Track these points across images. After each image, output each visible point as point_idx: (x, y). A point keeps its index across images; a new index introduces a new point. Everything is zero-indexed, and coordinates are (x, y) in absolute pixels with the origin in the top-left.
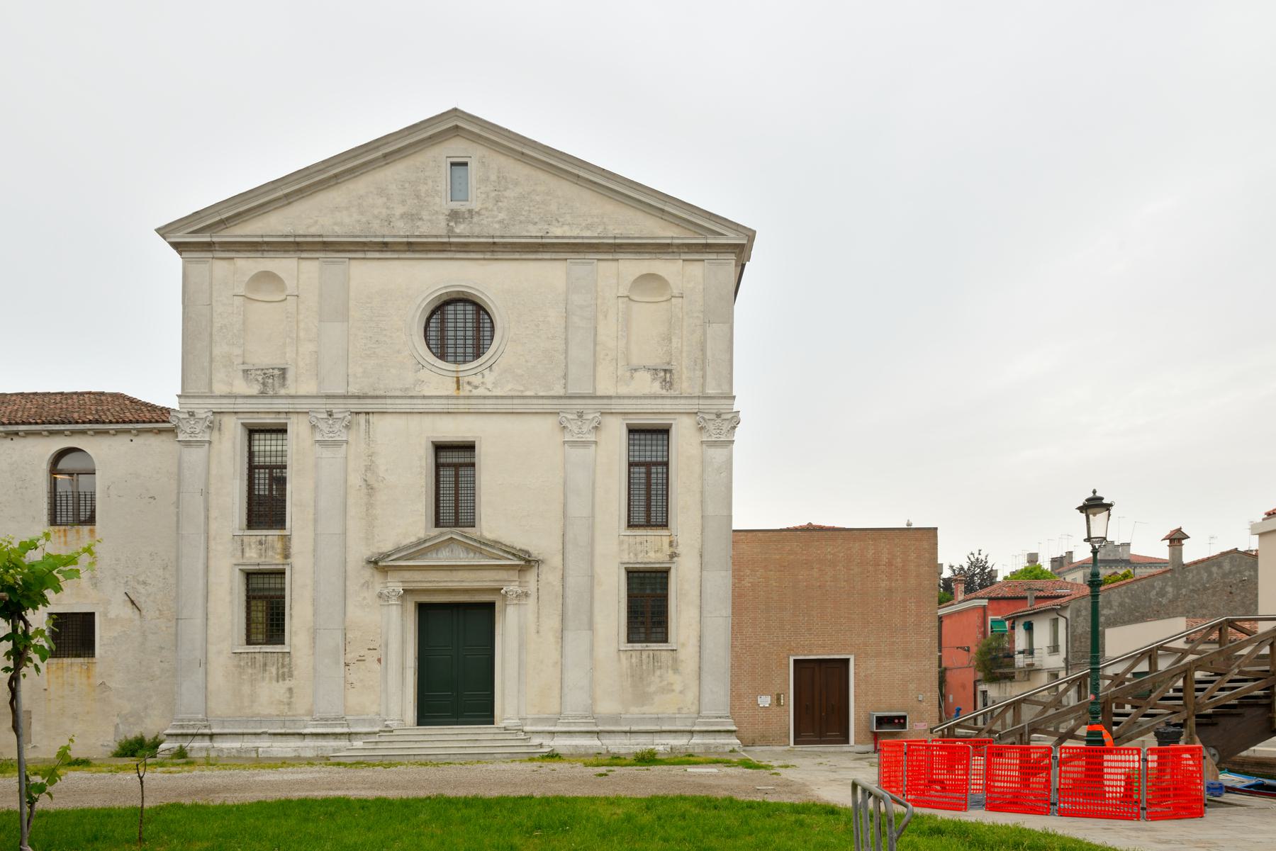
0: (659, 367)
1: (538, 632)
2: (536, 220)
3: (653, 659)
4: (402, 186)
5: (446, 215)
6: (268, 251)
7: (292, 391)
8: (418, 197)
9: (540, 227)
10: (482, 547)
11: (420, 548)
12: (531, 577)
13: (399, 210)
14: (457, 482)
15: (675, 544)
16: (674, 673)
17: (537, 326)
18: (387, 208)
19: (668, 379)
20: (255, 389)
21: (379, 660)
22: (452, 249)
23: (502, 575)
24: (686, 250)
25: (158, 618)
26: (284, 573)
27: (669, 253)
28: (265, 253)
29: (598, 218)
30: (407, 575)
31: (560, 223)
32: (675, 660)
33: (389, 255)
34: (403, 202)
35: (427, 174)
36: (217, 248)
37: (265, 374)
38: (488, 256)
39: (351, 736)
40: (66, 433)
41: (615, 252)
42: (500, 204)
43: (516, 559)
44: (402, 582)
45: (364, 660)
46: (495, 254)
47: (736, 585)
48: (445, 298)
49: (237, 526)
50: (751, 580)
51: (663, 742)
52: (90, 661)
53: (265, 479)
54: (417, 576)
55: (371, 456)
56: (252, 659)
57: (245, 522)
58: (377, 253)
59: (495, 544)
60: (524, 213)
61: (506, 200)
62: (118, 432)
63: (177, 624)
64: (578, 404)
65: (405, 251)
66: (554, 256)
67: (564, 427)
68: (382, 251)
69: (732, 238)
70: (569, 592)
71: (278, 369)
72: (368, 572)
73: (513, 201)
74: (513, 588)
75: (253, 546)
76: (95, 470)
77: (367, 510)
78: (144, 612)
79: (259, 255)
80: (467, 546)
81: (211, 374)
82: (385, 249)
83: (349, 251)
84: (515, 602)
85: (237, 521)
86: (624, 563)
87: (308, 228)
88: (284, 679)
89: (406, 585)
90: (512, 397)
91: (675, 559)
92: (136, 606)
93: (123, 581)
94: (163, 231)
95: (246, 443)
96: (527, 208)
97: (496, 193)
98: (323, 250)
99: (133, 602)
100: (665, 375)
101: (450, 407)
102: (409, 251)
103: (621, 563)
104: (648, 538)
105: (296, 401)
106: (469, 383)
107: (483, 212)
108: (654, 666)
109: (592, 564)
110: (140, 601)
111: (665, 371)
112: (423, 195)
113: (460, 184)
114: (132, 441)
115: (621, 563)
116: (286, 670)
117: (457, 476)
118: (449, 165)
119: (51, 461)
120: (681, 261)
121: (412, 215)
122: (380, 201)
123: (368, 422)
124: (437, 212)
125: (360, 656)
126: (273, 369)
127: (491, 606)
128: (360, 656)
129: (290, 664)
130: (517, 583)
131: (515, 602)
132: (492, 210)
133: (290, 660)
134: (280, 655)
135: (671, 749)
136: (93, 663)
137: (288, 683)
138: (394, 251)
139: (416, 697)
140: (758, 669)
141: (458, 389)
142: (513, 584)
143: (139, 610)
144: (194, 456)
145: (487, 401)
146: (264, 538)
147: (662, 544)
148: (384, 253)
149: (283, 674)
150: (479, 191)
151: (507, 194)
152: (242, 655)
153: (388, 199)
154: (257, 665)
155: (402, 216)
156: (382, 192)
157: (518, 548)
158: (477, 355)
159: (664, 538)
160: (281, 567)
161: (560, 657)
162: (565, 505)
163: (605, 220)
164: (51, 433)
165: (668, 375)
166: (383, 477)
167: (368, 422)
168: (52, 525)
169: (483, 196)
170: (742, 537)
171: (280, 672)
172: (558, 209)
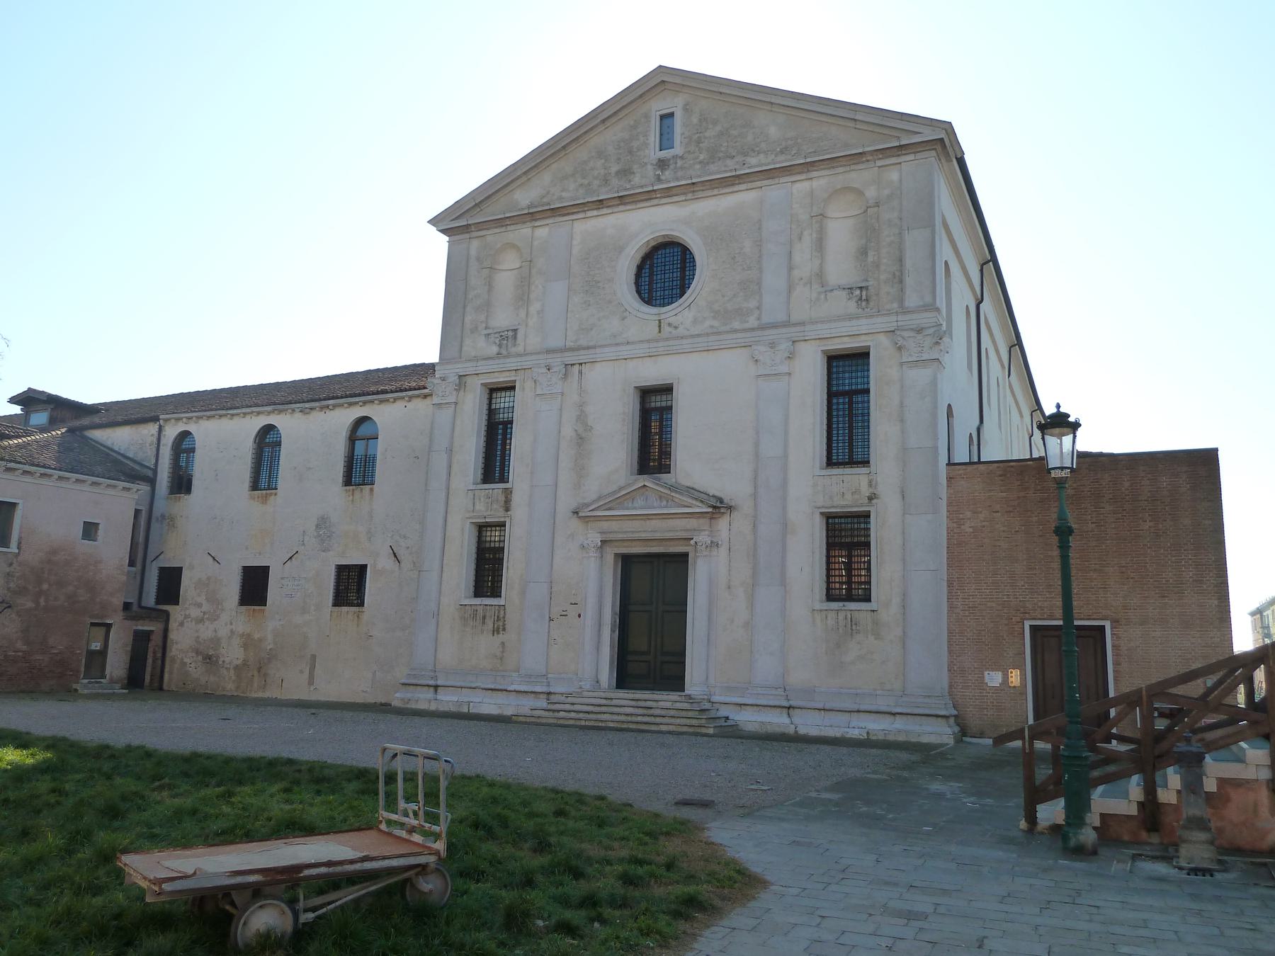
0: (854, 286)
1: (729, 588)
2: (734, 154)
3: (851, 621)
4: (618, 145)
6: (510, 225)
7: (520, 349)
9: (737, 160)
10: (673, 494)
11: (618, 499)
12: (723, 523)
13: (614, 169)
14: (851, 409)
15: (874, 483)
17: (734, 258)
18: (605, 169)
19: (864, 297)
20: (495, 349)
22: (658, 196)
23: (693, 523)
24: (881, 156)
26: (869, 516)
27: (863, 162)
28: (508, 227)
29: (792, 140)
30: (605, 525)
31: (756, 153)
32: (876, 623)
33: (605, 211)
35: (639, 130)
36: (473, 230)
37: (501, 336)
38: (690, 196)
40: (376, 402)
41: (808, 171)
42: (701, 145)
44: (600, 533)
45: (567, 615)
46: (696, 193)
47: (955, 531)
48: (653, 243)
49: (472, 481)
50: (973, 525)
51: (862, 725)
52: (361, 610)
54: (614, 525)
55: (582, 406)
57: (479, 476)
59: (690, 491)
60: (723, 149)
62: (335, 406)
63: (419, 575)
64: (772, 334)
65: (618, 205)
66: (750, 185)
67: (756, 360)
68: (599, 208)
69: (929, 135)
71: (512, 330)
72: (575, 523)
73: (712, 141)
74: (703, 538)
75: (482, 499)
76: (378, 435)
77: (576, 461)
78: (402, 564)
79: (503, 229)
81: (462, 342)
83: (573, 213)
84: (705, 553)
85: (471, 477)
86: (819, 508)
87: (541, 199)
88: (498, 633)
89: (604, 536)
91: (874, 501)
93: (390, 535)
94: (433, 222)
95: (486, 401)
96: (725, 144)
97: (698, 135)
98: (552, 217)
100: (861, 294)
101: (651, 350)
102: (621, 204)
103: (816, 507)
104: (845, 478)
106: (670, 325)
108: (852, 630)
109: (784, 508)
110: (400, 553)
111: (861, 288)
112: (635, 150)
114: (406, 406)
115: (816, 507)
116: (501, 623)
117: (851, 403)
118: (658, 118)
119: (350, 429)
120: (877, 168)
121: (625, 171)
122: (600, 163)
123: (580, 372)
124: (646, 164)
126: (507, 331)
127: (685, 556)
129: (504, 617)
130: (707, 533)
131: (705, 553)
132: (694, 153)
135: (868, 733)
136: (362, 612)
140: (985, 636)
141: (660, 332)
142: (703, 533)
144: (445, 416)
145: (684, 341)
147: (860, 484)
149: (498, 628)
150: (683, 136)
151: (707, 134)
152: (467, 607)
153: (606, 160)
155: (618, 173)
156: (600, 154)
157: (711, 495)
159: (861, 477)
162: (757, 445)
163: (799, 141)
164: (351, 404)
165: (864, 293)
166: (591, 426)
167: (580, 372)
169: (686, 140)
170: (960, 472)
171: (496, 626)
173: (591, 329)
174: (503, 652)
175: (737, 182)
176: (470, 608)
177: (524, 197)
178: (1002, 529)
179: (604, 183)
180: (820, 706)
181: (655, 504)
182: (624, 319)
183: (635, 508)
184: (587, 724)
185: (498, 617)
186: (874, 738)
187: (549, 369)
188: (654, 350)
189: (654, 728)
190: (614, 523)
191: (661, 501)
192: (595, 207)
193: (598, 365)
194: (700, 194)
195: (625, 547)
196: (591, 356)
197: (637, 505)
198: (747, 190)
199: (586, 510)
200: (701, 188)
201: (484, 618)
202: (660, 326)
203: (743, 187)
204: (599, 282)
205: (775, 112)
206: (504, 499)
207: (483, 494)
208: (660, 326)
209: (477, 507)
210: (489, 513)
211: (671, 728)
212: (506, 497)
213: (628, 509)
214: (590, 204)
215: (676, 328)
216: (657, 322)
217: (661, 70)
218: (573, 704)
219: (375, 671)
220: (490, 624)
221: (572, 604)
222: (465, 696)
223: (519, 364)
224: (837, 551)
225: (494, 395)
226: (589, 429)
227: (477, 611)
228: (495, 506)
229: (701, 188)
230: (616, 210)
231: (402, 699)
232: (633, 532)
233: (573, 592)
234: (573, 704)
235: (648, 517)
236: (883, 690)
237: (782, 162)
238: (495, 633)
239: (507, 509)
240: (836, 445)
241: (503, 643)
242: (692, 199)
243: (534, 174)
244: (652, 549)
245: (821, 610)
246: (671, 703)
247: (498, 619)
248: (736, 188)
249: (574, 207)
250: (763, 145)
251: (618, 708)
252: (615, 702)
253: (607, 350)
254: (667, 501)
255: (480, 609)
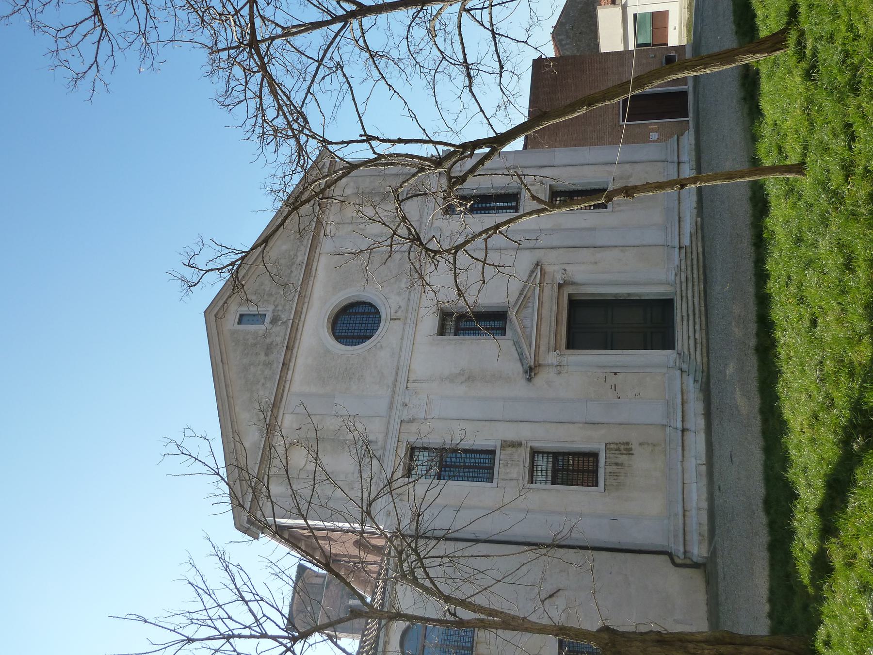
1: (596, 263)
2: (289, 271)
5: (273, 327)
7: (381, 437)
8: (255, 345)
13: (262, 357)
16: (632, 177)
21: (615, 374)
22: (297, 321)
25: (568, 573)
30: (543, 349)
33: (292, 364)
34: (257, 354)
39: (685, 482)
43: (536, 271)
44: (549, 352)
53: (451, 471)
56: (610, 476)
58: (289, 372)
61: (272, 290)
65: (292, 352)
66: (316, 260)
68: (288, 369)
70: (565, 244)
72: (540, 380)
78: (561, 586)
80: (522, 307)
82: (287, 366)
88: (631, 449)
89: (551, 349)
90: (400, 347)
92: (555, 593)
98: (278, 409)
99: (551, 596)
105: (390, 432)
106: (396, 312)
107: (276, 303)
113: (253, 320)
116: (622, 447)
122: (252, 369)
123: (414, 381)
125: (611, 388)
128: (611, 388)
129: (617, 444)
133: (613, 444)
134: (608, 451)
135: (692, 170)
137: (635, 446)
138: (290, 360)
139: (657, 92)
141: (400, 319)
143: (559, 590)
145: (412, 298)
146: (501, 462)
148: (290, 367)
149: (626, 449)
151: (267, 289)
152: (607, 483)
154: (617, 471)
155: (266, 355)
158: (377, 312)
160: (528, 449)
161: (617, 248)
167: (414, 381)
168: (502, 331)
172: (285, 258)
173: (382, 373)
174: (648, 444)
175: (310, 267)
176: (608, 481)
177: (252, 437)
178: (566, 137)
179: (269, 366)
180: (677, 202)
181: (530, 311)
182: (381, 347)
183: (532, 326)
184: (703, 305)
185: (616, 450)
186: (695, 166)
187: (406, 405)
188: (412, 320)
189: (701, 256)
190: (541, 342)
191: (529, 307)
192: (286, 371)
193: (412, 367)
194: (308, 293)
195: (561, 339)
196: (404, 369)
197: (530, 325)
198: (318, 262)
199: (529, 359)
200: (305, 291)
201: (617, 464)
202: (395, 319)
203: (315, 264)
204: (346, 369)
205: (273, 245)
206: (510, 449)
207: (504, 470)
208: (395, 319)
209: (515, 476)
210: (522, 463)
211: (700, 244)
212: (509, 446)
213: (531, 331)
214: (283, 374)
215: (400, 307)
216: (391, 321)
217: (208, 313)
218: (689, 337)
219: (674, 620)
220: (623, 458)
221: (605, 381)
222: (691, 475)
223: (394, 436)
224: (560, 463)
225: (416, 453)
226: (462, 373)
227: (610, 473)
228: (516, 457)
229: (305, 291)
230: (295, 355)
231: (700, 543)
232: (550, 326)
233: (596, 380)
234: (689, 337)
235: (540, 315)
236: (664, 172)
237: (308, 242)
238: (630, 452)
239: (520, 444)
240: (487, 457)
241: (641, 444)
242: (309, 299)
243: (236, 426)
244: (564, 320)
245: (613, 208)
246: (682, 273)
247: (618, 450)
248: (314, 269)
249: (279, 386)
250: (292, 253)
251: (689, 302)
252: (685, 314)
253: (402, 358)
254: (529, 302)
255: (609, 469)
